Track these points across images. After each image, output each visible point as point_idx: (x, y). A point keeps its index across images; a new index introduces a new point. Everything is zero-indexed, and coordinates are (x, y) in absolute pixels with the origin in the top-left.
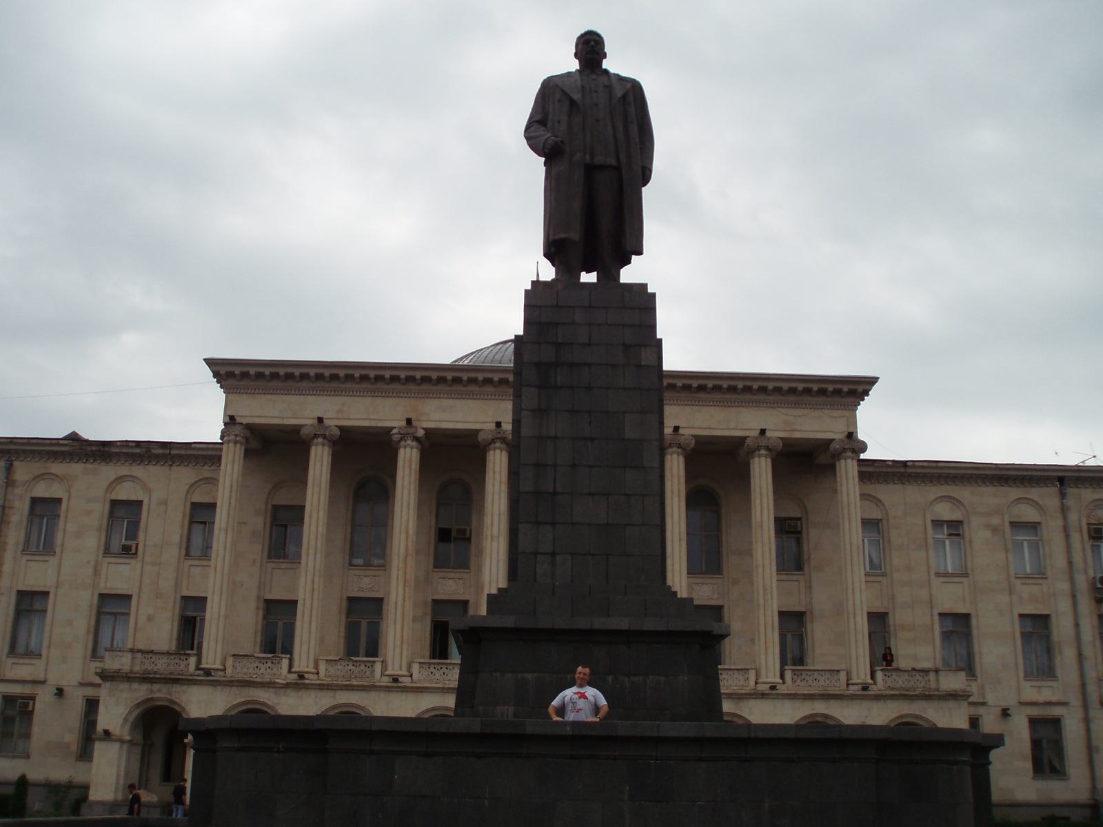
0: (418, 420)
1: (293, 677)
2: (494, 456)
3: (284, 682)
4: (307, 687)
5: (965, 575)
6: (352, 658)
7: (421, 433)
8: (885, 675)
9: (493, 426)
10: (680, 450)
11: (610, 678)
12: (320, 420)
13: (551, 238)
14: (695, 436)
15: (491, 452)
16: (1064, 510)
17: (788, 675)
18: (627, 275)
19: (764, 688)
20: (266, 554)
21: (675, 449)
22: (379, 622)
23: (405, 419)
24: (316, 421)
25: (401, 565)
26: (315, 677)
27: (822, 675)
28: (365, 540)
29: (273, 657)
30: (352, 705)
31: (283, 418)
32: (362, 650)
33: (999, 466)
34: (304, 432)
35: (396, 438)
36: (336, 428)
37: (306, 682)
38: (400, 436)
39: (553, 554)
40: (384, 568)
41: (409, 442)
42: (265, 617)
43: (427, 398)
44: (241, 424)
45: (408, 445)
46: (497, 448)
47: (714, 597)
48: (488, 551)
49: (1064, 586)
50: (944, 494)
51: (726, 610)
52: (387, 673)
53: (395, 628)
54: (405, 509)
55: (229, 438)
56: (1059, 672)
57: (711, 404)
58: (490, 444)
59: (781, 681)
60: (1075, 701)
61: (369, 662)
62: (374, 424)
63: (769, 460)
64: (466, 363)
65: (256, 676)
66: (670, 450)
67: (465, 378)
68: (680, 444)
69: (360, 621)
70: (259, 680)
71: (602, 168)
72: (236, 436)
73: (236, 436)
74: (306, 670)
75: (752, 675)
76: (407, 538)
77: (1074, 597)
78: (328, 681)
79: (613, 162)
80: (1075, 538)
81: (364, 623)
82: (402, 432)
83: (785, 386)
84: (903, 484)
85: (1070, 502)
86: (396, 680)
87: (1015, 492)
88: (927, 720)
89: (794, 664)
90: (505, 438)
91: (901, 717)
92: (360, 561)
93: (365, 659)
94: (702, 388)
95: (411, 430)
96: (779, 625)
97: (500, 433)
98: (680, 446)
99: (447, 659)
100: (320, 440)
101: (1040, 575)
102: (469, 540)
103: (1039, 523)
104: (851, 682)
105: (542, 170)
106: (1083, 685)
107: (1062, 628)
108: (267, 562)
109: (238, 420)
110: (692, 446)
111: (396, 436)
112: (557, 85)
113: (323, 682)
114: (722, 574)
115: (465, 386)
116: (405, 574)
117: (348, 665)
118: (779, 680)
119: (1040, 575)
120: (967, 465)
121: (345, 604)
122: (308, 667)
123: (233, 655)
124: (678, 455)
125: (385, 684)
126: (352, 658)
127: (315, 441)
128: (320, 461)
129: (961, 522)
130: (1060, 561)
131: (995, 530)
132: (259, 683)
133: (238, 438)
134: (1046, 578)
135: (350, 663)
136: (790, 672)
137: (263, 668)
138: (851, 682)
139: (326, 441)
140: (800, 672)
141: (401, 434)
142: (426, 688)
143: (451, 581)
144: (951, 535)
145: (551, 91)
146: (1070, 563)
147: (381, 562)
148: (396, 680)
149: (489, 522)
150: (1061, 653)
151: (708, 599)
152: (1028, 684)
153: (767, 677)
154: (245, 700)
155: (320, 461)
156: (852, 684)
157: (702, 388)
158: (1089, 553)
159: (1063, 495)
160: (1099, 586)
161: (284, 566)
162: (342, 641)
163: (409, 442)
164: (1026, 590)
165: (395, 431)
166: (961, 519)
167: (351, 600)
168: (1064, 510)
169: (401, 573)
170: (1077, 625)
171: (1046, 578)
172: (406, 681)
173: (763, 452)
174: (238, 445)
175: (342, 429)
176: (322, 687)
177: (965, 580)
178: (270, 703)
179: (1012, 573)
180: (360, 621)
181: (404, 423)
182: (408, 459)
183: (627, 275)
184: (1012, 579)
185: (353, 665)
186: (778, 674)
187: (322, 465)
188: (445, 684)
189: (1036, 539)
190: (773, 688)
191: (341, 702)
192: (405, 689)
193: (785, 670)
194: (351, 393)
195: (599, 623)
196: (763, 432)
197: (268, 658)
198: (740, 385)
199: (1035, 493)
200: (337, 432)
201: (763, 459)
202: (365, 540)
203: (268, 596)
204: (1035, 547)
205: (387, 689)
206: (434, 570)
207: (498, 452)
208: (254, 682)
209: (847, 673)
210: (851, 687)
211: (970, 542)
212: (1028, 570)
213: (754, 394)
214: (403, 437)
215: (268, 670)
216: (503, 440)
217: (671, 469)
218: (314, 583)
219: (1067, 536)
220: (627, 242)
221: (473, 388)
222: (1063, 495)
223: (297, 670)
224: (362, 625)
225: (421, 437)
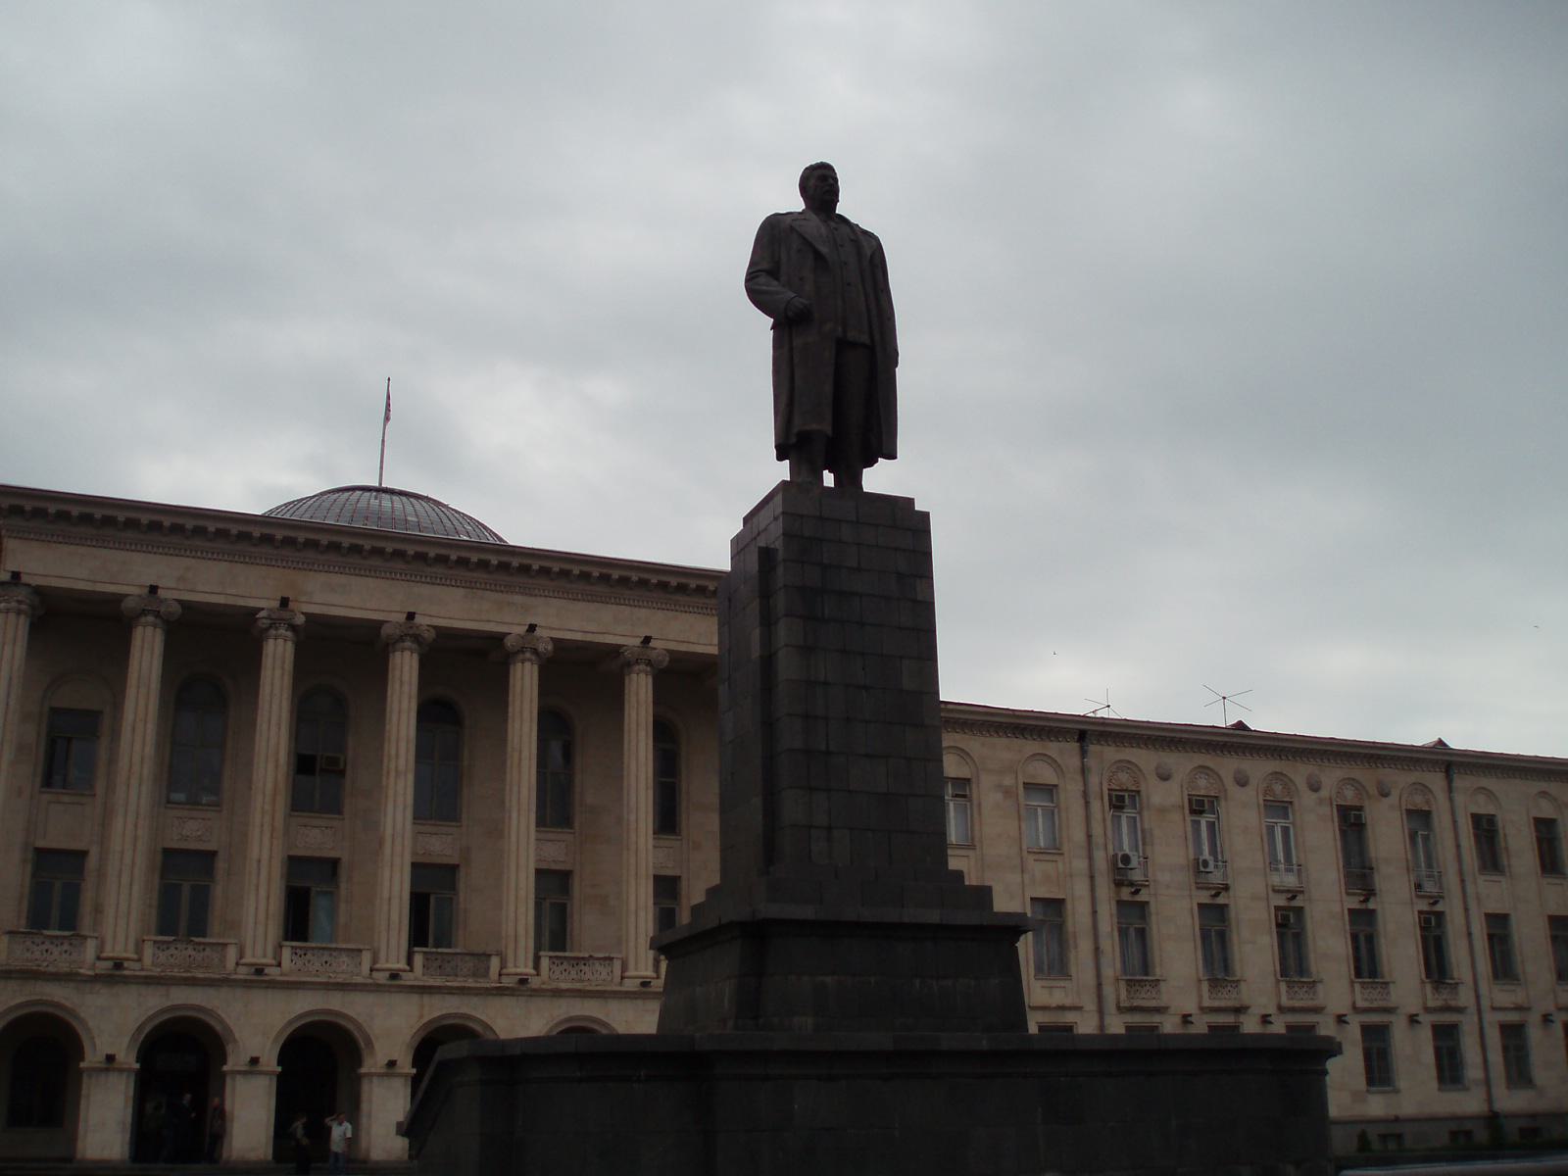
0: (296, 601)
1: (104, 967)
2: (276, 646)
3: (91, 973)
4: (126, 981)
5: (971, 847)
6: (193, 938)
7: (300, 620)
8: (296, 954)
9: (402, 618)
10: (649, 669)
11: (917, 982)
12: (153, 589)
13: (798, 424)
14: (670, 652)
15: (398, 654)
16: (1084, 771)
17: (545, 963)
18: (877, 479)
19: (382, 978)
20: (38, 780)
21: (642, 667)
22: (451, 899)
23: (279, 598)
24: (146, 590)
25: (267, 807)
26: (137, 966)
27: (57, 945)
28: (196, 767)
29: (72, 935)
30: (193, 1007)
31: (95, 582)
32: (431, 940)
33: (1017, 713)
34: (128, 604)
35: (264, 623)
36: (176, 603)
37: (126, 972)
38: (269, 621)
39: (829, 829)
40: (218, 808)
41: (282, 631)
42: (34, 875)
43: (310, 570)
44: (29, 585)
45: (281, 635)
46: (406, 649)
47: (670, 866)
48: (391, 792)
49: (1080, 865)
50: (952, 744)
51: (684, 883)
52: (243, 961)
53: (257, 895)
54: (274, 729)
55: (8, 606)
56: (1073, 970)
57: (362, 572)
58: (397, 641)
59: (408, 968)
60: (1090, 1005)
61: (301, 948)
62: (231, 601)
63: (415, 656)
64: (287, 516)
65: (45, 964)
66: (636, 668)
67: (212, 529)
68: (159, 612)
69: (181, 885)
70: (51, 969)
71: (854, 345)
72: (19, 602)
73: (19, 602)
74: (125, 955)
75: (366, 958)
76: (277, 767)
77: (1092, 878)
78: (156, 971)
79: (865, 339)
80: (1096, 806)
81: (186, 888)
82: (274, 616)
83: (98, 513)
84: (1042, 739)
85: (1091, 762)
86: (259, 971)
87: (1031, 746)
88: (605, 1025)
89: (552, 949)
90: (419, 635)
91: (570, 1019)
92: (181, 797)
93: (58, 933)
94: (682, 588)
95: (286, 615)
96: (536, 889)
97: (411, 627)
98: (649, 663)
99: (204, 936)
100: (150, 619)
101: (1054, 849)
102: (342, 773)
103: (1056, 786)
104: (627, 974)
105: (769, 336)
106: (1099, 985)
107: (1078, 916)
108: (41, 792)
109: (25, 579)
110: (665, 664)
111: (265, 621)
112: (792, 229)
113: (149, 973)
114: (680, 835)
115: (255, 545)
116: (273, 819)
117: (186, 949)
118: (402, 965)
119: (1054, 849)
120: (980, 709)
121: (159, 858)
122: (126, 951)
123: (10, 933)
124: (412, 653)
125: (242, 977)
126: (193, 938)
127: (143, 620)
128: (147, 652)
129: (968, 780)
130: (1078, 835)
131: (1008, 792)
132: (51, 974)
133: (23, 607)
134: (1062, 854)
135: (190, 947)
136: (547, 959)
137: (56, 951)
138: (627, 974)
139: (158, 621)
140: (202, 947)
141: (272, 619)
142: (304, 983)
143: (317, 831)
144: (957, 796)
145: (774, 233)
146: (1089, 836)
147: (213, 798)
148: (259, 971)
149: (393, 752)
150: (1076, 947)
151: (662, 867)
152: (1039, 984)
153: (387, 961)
154: (28, 999)
155: (147, 652)
156: (508, 975)
157: (682, 588)
158: (1109, 823)
159: (1083, 753)
160: (1121, 865)
161: (66, 799)
162: (154, 912)
163: (282, 631)
164: (1038, 868)
165: (262, 614)
166: (969, 777)
167: (169, 853)
168: (1084, 771)
169: (267, 819)
170: (1094, 912)
171: (1062, 854)
172: (273, 973)
173: (528, 655)
174: (22, 617)
175: (185, 605)
176: (149, 981)
177: (970, 853)
178: (68, 1004)
179: (1024, 847)
180: (181, 885)
181: (276, 604)
182: (278, 656)
183: (877, 479)
184: (1025, 853)
185: (195, 949)
186: (531, 964)
187: (152, 653)
188: (330, 977)
189: (1051, 805)
190: (645, 984)
191: (176, 1002)
192: (273, 985)
193: (414, 952)
194: (321, 568)
195: (910, 915)
196: (647, 640)
197: (65, 937)
198: (212, 527)
199: (1053, 748)
200: (177, 609)
201: (407, 654)
202: (196, 767)
203: (41, 844)
204: (1050, 814)
205: (247, 984)
206: (293, 813)
207: (407, 654)
208: (44, 973)
209: (623, 962)
210: (375, 974)
211: (979, 805)
212: (1042, 844)
213: (365, 558)
214: (274, 623)
215: (64, 956)
216: (417, 638)
217: (637, 694)
218: (126, 828)
219: (1087, 803)
220: (877, 438)
221: (376, 562)
222: (1083, 753)
223: (111, 955)
224: (186, 891)
225: (298, 626)
